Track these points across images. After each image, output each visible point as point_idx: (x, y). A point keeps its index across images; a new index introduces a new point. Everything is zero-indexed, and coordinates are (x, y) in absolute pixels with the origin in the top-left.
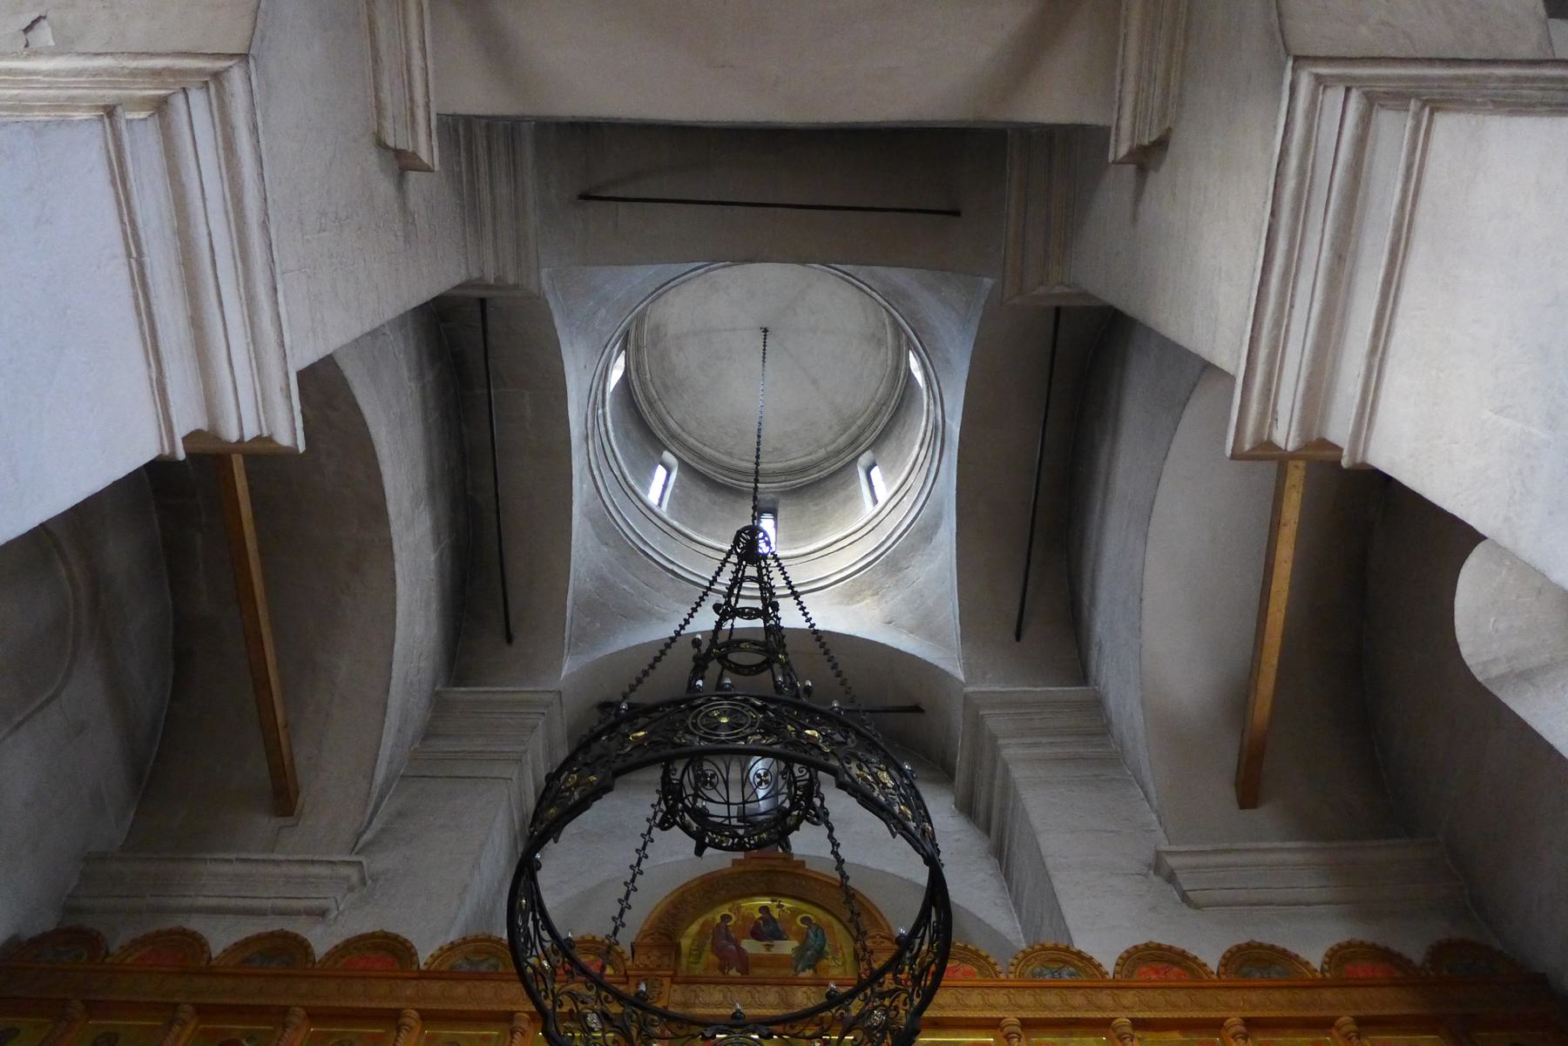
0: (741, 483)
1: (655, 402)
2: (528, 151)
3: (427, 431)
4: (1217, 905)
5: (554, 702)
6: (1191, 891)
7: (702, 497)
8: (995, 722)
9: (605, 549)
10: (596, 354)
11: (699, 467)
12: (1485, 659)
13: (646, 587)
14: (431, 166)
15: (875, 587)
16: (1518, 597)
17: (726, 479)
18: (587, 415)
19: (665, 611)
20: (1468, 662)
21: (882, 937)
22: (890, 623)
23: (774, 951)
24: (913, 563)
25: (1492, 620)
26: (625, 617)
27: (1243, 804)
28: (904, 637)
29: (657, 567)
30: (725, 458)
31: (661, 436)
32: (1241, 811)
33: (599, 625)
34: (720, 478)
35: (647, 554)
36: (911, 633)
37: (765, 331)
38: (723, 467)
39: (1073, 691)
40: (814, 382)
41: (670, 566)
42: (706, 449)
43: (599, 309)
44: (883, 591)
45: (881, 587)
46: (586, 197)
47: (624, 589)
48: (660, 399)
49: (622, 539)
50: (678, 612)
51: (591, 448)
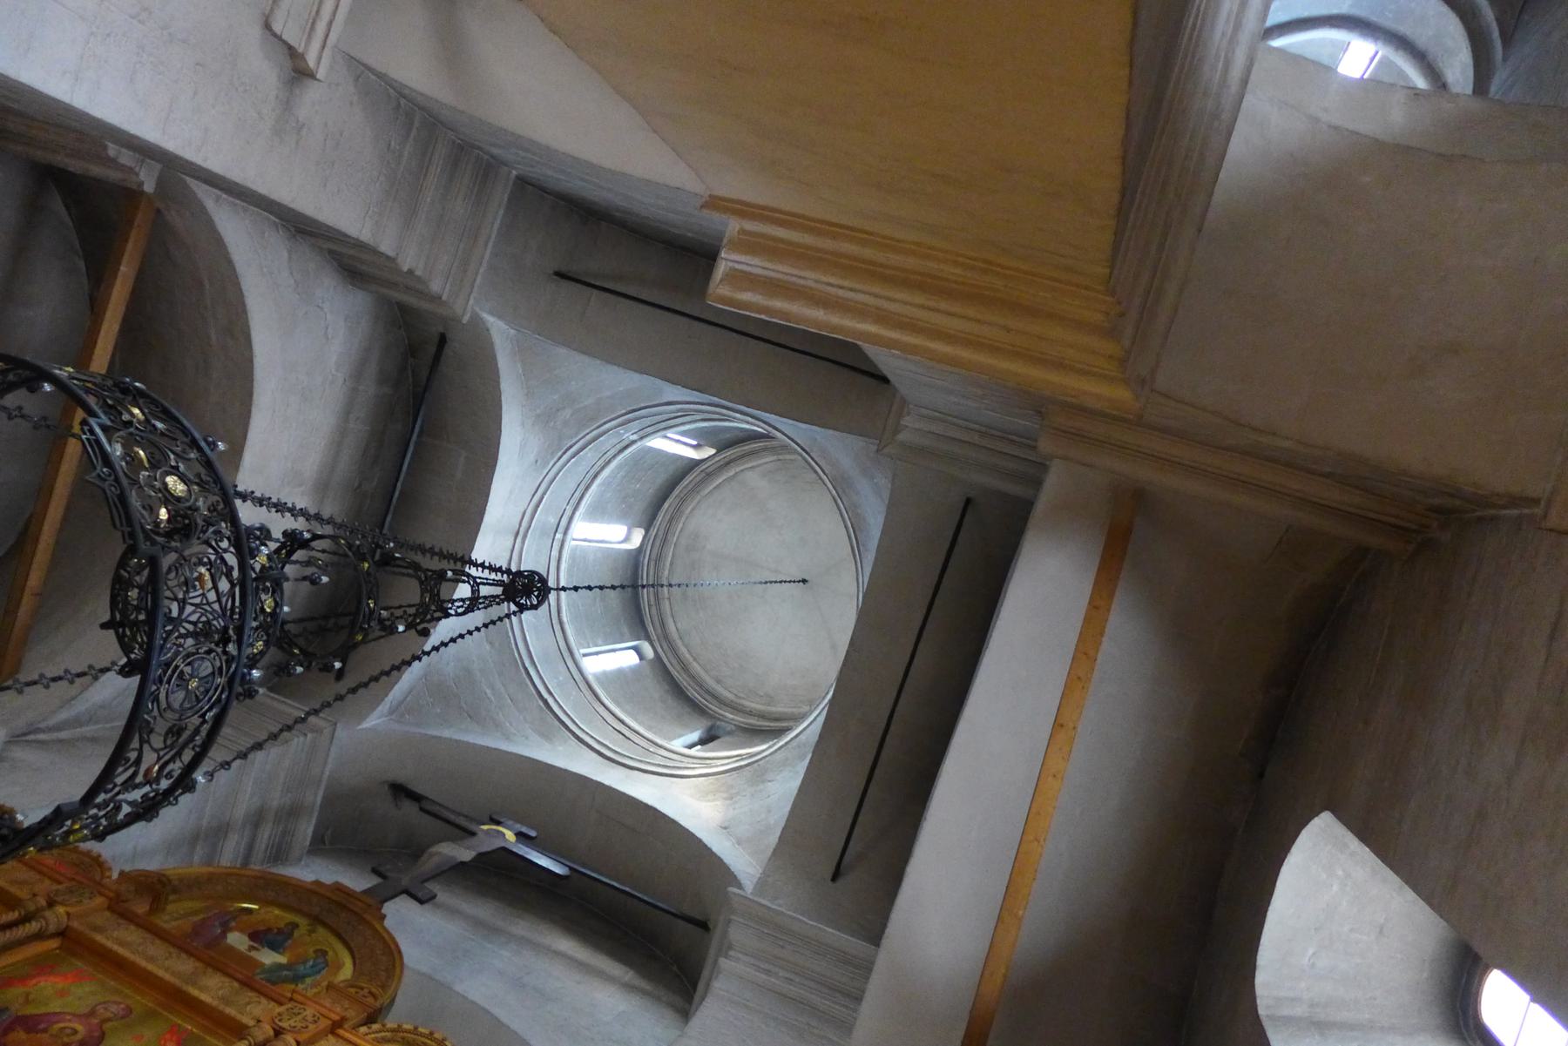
0: (710, 706)
1: (663, 599)
2: (500, 196)
3: (341, 432)
5: (325, 731)
7: (654, 689)
8: (738, 933)
9: (488, 647)
10: (553, 454)
11: (675, 673)
13: (509, 701)
14: (315, 72)
15: (734, 791)
16: (1352, 930)
19: (513, 730)
21: (370, 993)
22: (725, 828)
23: (253, 954)
24: (778, 777)
25: (1311, 952)
26: (471, 717)
28: (728, 844)
30: (710, 682)
31: (650, 628)
34: (692, 693)
37: (804, 581)
38: (701, 686)
39: (854, 945)
41: (546, 695)
42: (695, 664)
43: (564, 408)
44: (739, 797)
45: (738, 793)
46: (561, 275)
47: (486, 693)
48: (669, 599)
50: (527, 738)
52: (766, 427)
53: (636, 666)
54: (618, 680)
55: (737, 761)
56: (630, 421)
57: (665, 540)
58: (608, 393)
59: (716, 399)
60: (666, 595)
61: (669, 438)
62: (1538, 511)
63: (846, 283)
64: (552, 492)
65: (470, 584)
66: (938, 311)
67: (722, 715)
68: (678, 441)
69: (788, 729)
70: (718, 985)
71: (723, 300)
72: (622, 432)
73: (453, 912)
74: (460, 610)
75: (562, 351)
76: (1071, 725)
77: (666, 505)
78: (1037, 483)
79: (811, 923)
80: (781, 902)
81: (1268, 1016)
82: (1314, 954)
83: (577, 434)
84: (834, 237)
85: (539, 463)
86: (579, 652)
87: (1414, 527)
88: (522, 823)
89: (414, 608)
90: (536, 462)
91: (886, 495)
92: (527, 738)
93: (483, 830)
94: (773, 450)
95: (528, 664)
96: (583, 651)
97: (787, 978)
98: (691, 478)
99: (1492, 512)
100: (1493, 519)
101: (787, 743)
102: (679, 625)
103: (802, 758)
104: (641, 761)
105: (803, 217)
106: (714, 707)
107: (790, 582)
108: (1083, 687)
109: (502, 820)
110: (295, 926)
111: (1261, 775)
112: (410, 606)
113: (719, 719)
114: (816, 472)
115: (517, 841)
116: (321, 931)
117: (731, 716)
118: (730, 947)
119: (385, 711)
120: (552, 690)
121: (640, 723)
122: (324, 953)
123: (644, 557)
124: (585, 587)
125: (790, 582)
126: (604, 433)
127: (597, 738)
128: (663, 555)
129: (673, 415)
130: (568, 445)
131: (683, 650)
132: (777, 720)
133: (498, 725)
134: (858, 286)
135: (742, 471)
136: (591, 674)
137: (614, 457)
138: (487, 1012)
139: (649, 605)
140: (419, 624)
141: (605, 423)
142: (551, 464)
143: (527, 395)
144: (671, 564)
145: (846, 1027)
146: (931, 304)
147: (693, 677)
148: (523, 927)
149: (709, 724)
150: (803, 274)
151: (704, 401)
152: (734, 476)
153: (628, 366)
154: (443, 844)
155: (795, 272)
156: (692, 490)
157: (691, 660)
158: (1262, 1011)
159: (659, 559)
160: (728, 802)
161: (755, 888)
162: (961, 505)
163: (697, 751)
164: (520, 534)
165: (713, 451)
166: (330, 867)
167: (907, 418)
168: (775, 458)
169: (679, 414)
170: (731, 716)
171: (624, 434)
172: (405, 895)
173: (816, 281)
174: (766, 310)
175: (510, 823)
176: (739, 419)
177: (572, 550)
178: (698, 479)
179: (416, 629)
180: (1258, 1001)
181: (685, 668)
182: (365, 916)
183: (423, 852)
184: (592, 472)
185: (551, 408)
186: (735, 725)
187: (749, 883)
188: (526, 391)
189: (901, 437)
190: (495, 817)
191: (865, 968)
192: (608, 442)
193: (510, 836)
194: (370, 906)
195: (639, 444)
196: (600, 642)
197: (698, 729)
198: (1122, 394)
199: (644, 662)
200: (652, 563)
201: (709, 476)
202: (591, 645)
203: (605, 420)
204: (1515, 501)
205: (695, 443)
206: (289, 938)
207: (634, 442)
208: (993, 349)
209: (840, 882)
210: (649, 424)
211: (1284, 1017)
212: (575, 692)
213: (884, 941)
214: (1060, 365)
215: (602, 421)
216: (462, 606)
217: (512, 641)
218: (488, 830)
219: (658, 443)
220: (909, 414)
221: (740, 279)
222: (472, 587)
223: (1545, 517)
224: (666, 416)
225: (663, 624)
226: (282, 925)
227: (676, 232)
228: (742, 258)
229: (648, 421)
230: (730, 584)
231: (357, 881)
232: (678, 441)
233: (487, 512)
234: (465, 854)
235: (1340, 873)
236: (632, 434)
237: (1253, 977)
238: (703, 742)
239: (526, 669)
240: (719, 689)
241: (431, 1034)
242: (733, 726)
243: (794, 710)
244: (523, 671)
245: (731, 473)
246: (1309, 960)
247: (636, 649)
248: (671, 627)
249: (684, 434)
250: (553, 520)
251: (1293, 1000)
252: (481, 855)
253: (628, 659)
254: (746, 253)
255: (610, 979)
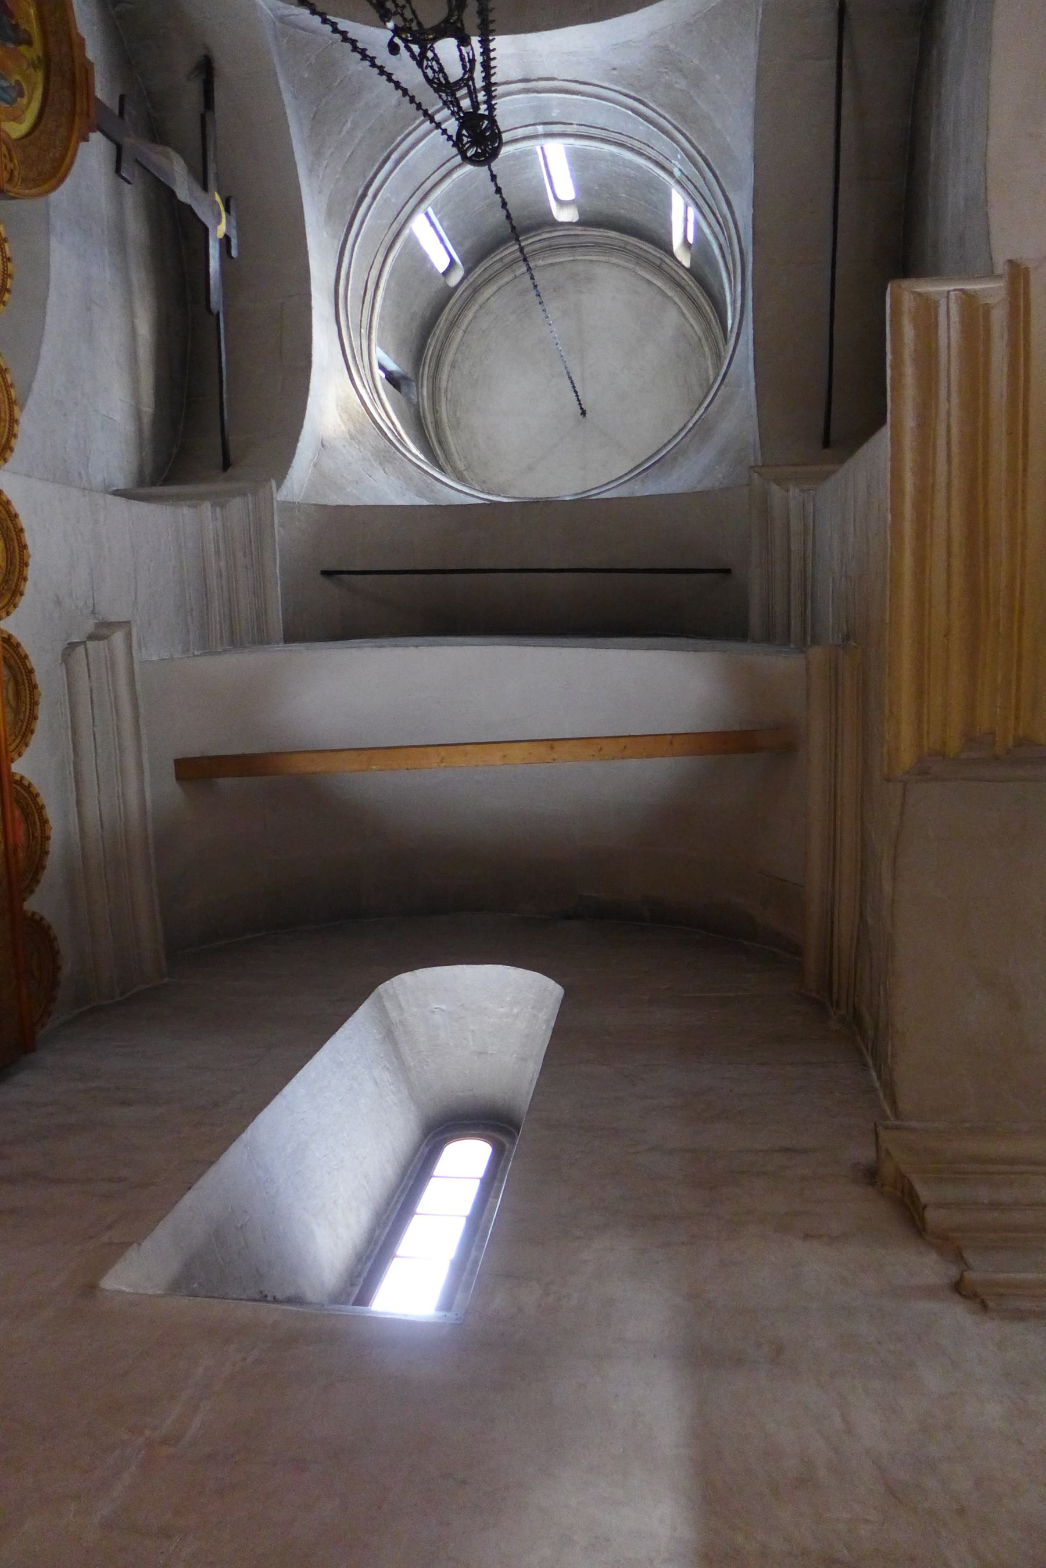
0: (427, 364)
4: (70, 685)
6: (86, 650)
7: (420, 303)
10: (630, 85)
12: (401, 997)
15: (360, 438)
16: (473, 1031)
17: (431, 349)
18: (553, 79)
20: (396, 980)
22: (323, 446)
24: (392, 478)
25: (443, 1007)
26: (314, 118)
27: (178, 762)
29: (371, 174)
31: (479, 270)
32: (172, 762)
33: (306, 76)
34: (432, 342)
35: (385, 162)
36: (315, 465)
37: (584, 413)
38: (441, 349)
40: (530, 469)
42: (460, 333)
43: (685, 77)
44: (357, 447)
45: (359, 443)
47: (344, 124)
48: (516, 277)
49: (403, 129)
50: (320, 192)
51: (513, 87)
52: (735, 331)
53: (438, 272)
54: (417, 257)
55: (390, 429)
56: (695, 164)
57: (572, 247)
58: (719, 126)
59: (750, 258)
60: (518, 273)
61: (686, 212)
62: (892, 1121)
63: (955, 449)
64: (585, 101)
65: (464, 74)
66: (949, 554)
67: (422, 385)
68: (686, 220)
69: (442, 470)
70: (186, 512)
71: (897, 302)
72: (679, 156)
73: (118, 196)
74: (429, 72)
75: (752, 48)
76: (555, 756)
77: (613, 234)
78: (768, 637)
79: (278, 572)
80: (282, 532)
81: (379, 994)
82: (443, 1010)
83: (661, 105)
84: (1011, 432)
85: (615, 72)
86: (428, 206)
87: (835, 996)
88: (239, 238)
89: (411, 16)
90: (615, 69)
91: (707, 484)
92: (320, 192)
93: (214, 196)
94: (708, 328)
95: (394, 156)
96: (430, 211)
97: (220, 571)
98: (650, 250)
99: (870, 1062)
100: (865, 1065)
101: (426, 472)
102: (493, 299)
103: (420, 493)
104: (350, 337)
105: (1027, 389)
106: (426, 371)
107: (579, 400)
108: (593, 756)
109: (233, 212)
110: (29, 43)
111: (568, 917)
112: (413, 12)
113: (417, 382)
114: (705, 397)
115: (220, 239)
116: (39, 77)
117: (425, 394)
118: (223, 506)
119: (279, 12)
120: (379, 197)
121: (383, 307)
122: (21, 94)
123: (549, 232)
124: (503, 200)
125: (579, 400)
126: (673, 139)
127: (352, 270)
128: (560, 251)
129: (715, 208)
130: (645, 100)
131: (470, 315)
132: (440, 442)
133: (318, 154)
134: (955, 460)
135: (675, 303)
136: (411, 229)
137: (649, 158)
138: (47, 288)
139: (501, 259)
140: (401, 38)
141: (683, 134)
142: (616, 88)
143: (688, 24)
144: (552, 264)
145: (207, 648)
146: (956, 549)
147: (447, 336)
148: (140, 277)
149: (410, 375)
150: (954, 397)
151: (743, 244)
152: (668, 297)
153: (758, 137)
154: (182, 162)
155: (954, 387)
156: (638, 257)
157: (463, 327)
158: (381, 988)
159: (553, 248)
160: (348, 437)
161: (284, 502)
162: (721, 566)
163: (381, 377)
164: (528, 83)
165: (686, 262)
166: (95, 28)
167: (797, 490)
168: (700, 334)
169: (721, 220)
170: (425, 394)
171: (677, 159)
172: (115, 147)
173: (949, 413)
174: (897, 366)
175: (234, 223)
176: (735, 292)
177: (530, 150)
178: (650, 257)
179: (393, 37)
180: (388, 982)
181: (453, 324)
182: (77, 119)
183: (166, 143)
184: (623, 138)
185: (680, 61)
186: (418, 402)
187: (285, 493)
188: (691, 21)
189: (774, 487)
190: (232, 203)
191: (261, 639)
192: (662, 145)
193: (221, 230)
194: (88, 115)
195: (671, 181)
196: (446, 224)
197: (400, 367)
198: (907, 758)
199: (443, 278)
200: (546, 243)
201: (659, 269)
202: (439, 216)
203: (688, 134)
204: (889, 1086)
205: (691, 239)
206: (14, 43)
207: (671, 174)
208: (921, 618)
209: (324, 581)
210: (697, 185)
211: (384, 1006)
212: (386, 222)
213: (295, 647)
214: (921, 693)
215: (684, 131)
216: (434, 71)
217: (411, 128)
218: (216, 202)
219: (678, 200)
220: (803, 491)
221: (928, 308)
222: (462, 79)
223: (887, 1128)
224: (712, 202)
225: (487, 282)
226: (23, 26)
227: (932, 139)
228: (955, 317)
229: (700, 183)
230: (557, 344)
231: (103, 89)
232: (686, 220)
233: (539, 34)
234: (184, 190)
235: (515, 1011)
236: (680, 170)
237: (405, 972)
238: (392, 378)
239: (388, 157)
240: (446, 369)
241: (9, 259)
242: (416, 400)
243: (456, 454)
244: (385, 154)
245: (670, 293)
246: (436, 1008)
247: (452, 262)
248: (488, 292)
249: (697, 224)
250: (555, 114)
251: (400, 1006)
252: (189, 207)
253: (441, 263)
254: (962, 322)
255: (135, 393)
